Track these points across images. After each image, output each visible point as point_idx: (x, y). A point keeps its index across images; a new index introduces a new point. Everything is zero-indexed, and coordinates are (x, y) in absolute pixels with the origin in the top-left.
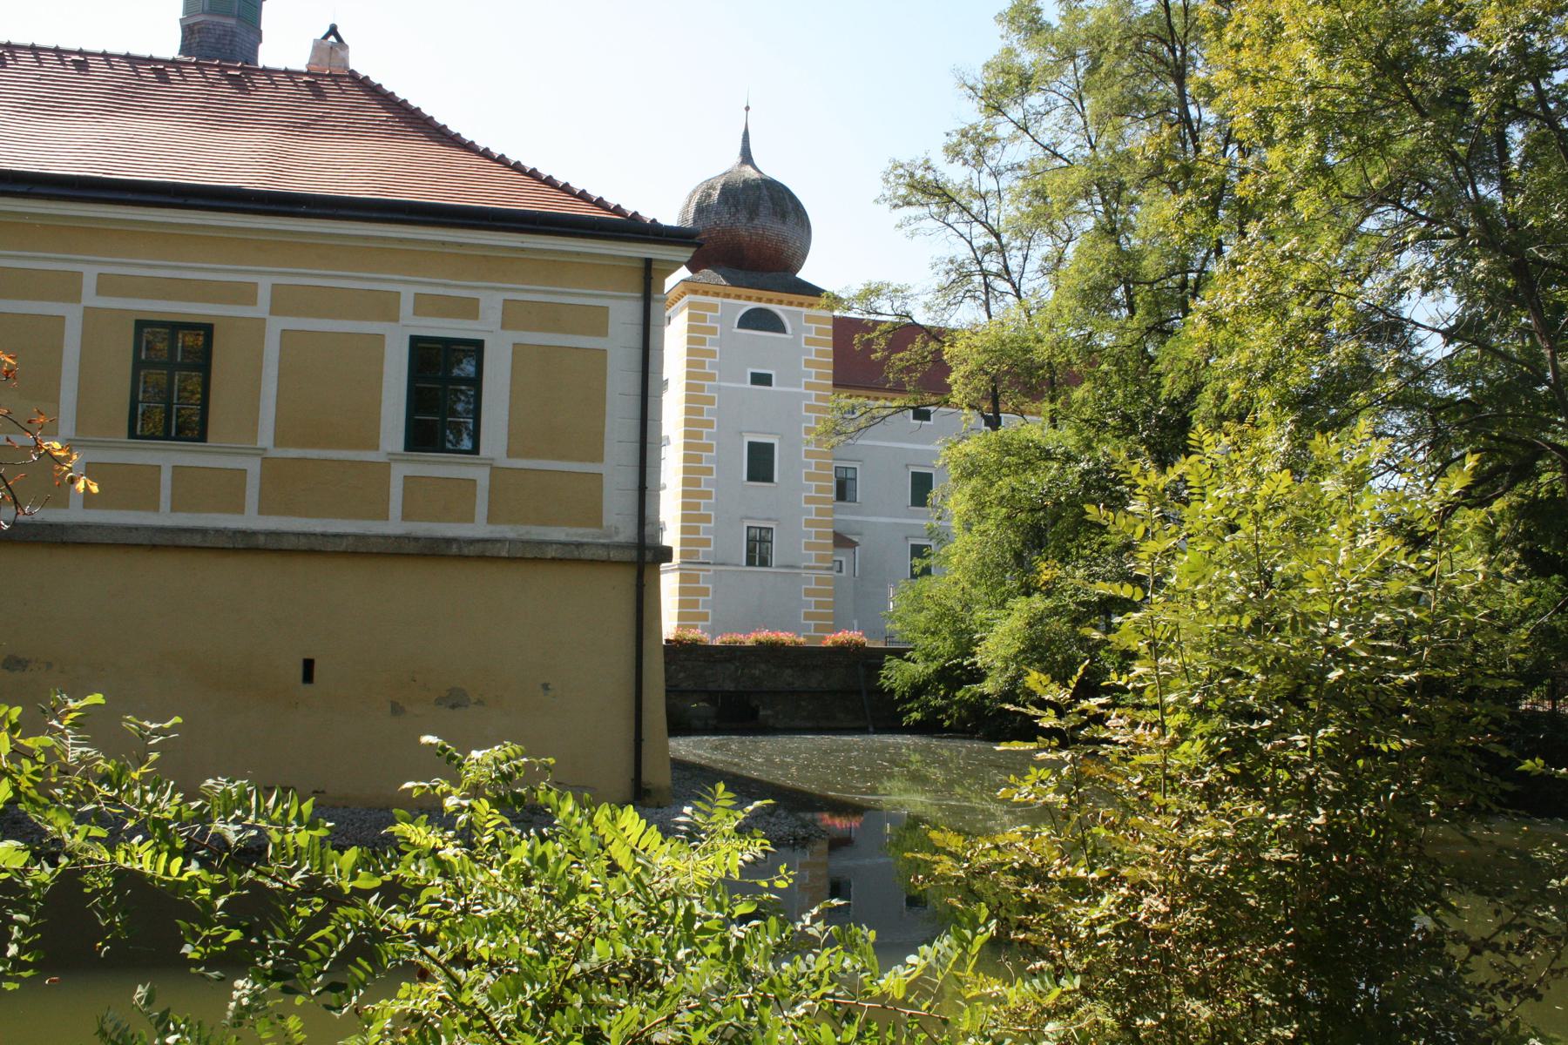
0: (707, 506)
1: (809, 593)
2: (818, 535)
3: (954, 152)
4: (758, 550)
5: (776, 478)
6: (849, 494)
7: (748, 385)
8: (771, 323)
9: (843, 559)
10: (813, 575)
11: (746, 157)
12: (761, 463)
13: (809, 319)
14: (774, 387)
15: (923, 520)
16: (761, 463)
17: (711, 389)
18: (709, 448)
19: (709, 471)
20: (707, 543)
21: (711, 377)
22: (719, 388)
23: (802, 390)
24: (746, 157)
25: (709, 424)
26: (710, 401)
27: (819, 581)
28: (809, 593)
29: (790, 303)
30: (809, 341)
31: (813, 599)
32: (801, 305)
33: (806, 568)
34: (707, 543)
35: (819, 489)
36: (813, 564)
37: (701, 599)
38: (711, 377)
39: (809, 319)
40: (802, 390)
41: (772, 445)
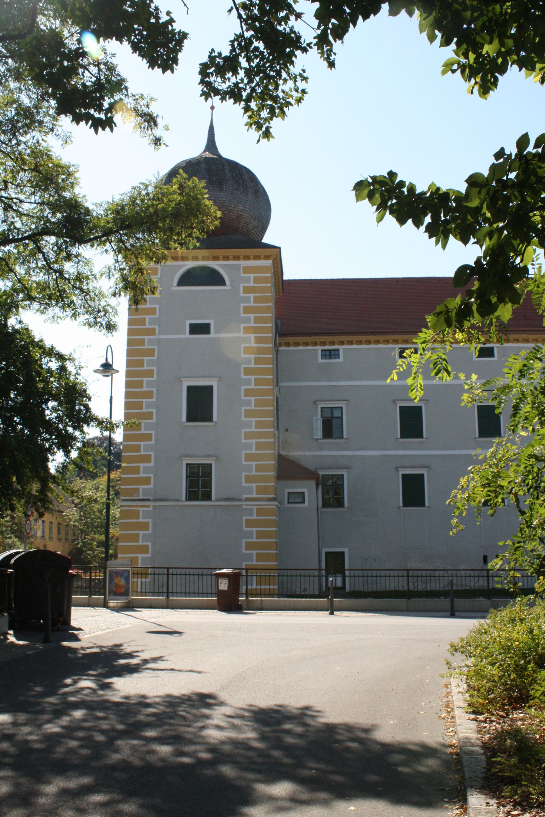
0: (147, 448)
1: (249, 523)
2: (259, 468)
3: (155, 7)
4: (199, 482)
5: (215, 418)
6: (335, 431)
7: (187, 335)
8: (213, 278)
9: (305, 490)
10: (254, 506)
11: (211, 145)
12: (200, 404)
13: (247, 270)
14: (212, 335)
15: (412, 451)
16: (200, 404)
17: (150, 342)
18: (149, 395)
19: (149, 416)
20: (147, 481)
21: (151, 332)
22: (159, 341)
23: (241, 334)
24: (211, 145)
25: (149, 374)
26: (151, 353)
27: (260, 512)
28: (249, 523)
29: (226, 258)
30: (247, 290)
31: (254, 530)
32: (237, 258)
33: (247, 500)
34: (147, 481)
35: (258, 425)
36: (254, 495)
37: (141, 533)
38: (151, 332)
39: (247, 270)
40: (241, 334)
41: (211, 388)
